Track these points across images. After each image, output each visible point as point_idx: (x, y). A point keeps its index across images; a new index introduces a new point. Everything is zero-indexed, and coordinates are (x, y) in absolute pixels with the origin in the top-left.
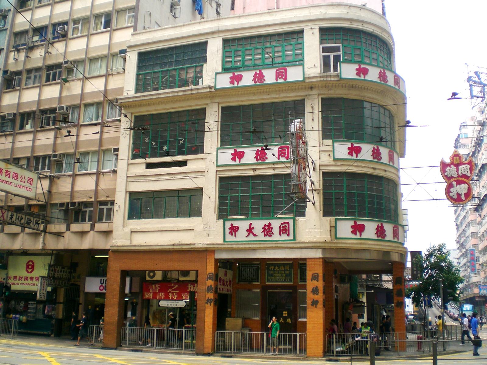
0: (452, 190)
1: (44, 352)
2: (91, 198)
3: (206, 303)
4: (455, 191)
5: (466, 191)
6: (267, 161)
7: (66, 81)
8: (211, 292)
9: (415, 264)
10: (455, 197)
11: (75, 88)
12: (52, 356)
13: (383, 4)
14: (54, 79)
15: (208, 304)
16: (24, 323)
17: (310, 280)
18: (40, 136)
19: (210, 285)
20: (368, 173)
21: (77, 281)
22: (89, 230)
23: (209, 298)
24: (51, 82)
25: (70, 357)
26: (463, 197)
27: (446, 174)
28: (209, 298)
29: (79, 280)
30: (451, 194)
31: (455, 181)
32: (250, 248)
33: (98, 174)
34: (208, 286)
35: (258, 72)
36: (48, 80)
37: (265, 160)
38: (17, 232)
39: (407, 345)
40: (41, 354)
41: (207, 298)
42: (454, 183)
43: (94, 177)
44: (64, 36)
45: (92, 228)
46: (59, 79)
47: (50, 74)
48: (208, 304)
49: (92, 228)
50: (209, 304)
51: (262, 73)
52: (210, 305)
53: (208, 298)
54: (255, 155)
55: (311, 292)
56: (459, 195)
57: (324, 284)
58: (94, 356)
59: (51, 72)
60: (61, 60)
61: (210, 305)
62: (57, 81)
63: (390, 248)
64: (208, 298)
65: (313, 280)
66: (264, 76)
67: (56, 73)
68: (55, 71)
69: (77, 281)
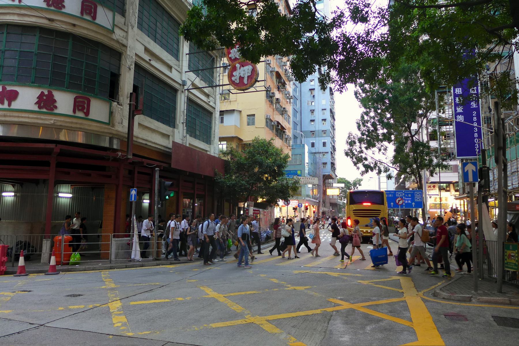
0: (234, 73)
4: (238, 74)
5: (249, 74)
6: (56, 111)
10: (238, 81)
16: (413, 122)
20: (121, 84)
26: (245, 81)
27: (230, 56)
30: (233, 79)
31: (239, 63)
32: (2, 121)
35: (46, 93)
37: (53, 110)
39: (432, 250)
42: (238, 65)
51: (53, 96)
54: (37, 100)
56: (241, 78)
65: (77, 111)
66: (55, 101)
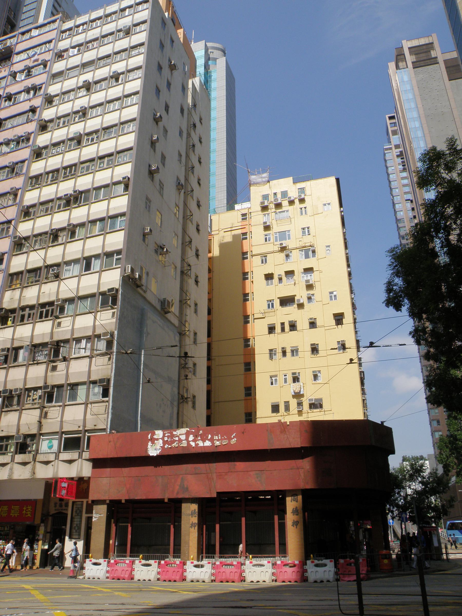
1: (26, 584)
2: (79, 427)
3: (190, 527)
7: (57, 317)
8: (195, 516)
9: (439, 213)
11: (66, 322)
12: (36, 589)
13: (350, 284)
14: (47, 316)
15: (192, 528)
17: (290, 501)
18: (31, 368)
19: (193, 509)
21: (64, 510)
22: (77, 458)
23: (193, 523)
24: (44, 319)
25: (54, 588)
28: (193, 523)
29: (66, 508)
33: (86, 404)
34: (192, 511)
36: (41, 317)
38: (7, 462)
40: (25, 587)
41: (191, 523)
43: (83, 406)
44: (57, 276)
45: (13, 459)
46: (51, 316)
47: (43, 311)
48: (192, 528)
49: (13, 459)
50: (193, 528)
52: (194, 529)
53: (192, 522)
55: (291, 513)
57: (285, 515)
58: (80, 586)
59: (44, 310)
60: (53, 298)
61: (194, 529)
62: (49, 318)
63: (220, 588)
64: (192, 522)
65: (293, 501)
67: (48, 310)
68: (47, 308)
69: (64, 510)
